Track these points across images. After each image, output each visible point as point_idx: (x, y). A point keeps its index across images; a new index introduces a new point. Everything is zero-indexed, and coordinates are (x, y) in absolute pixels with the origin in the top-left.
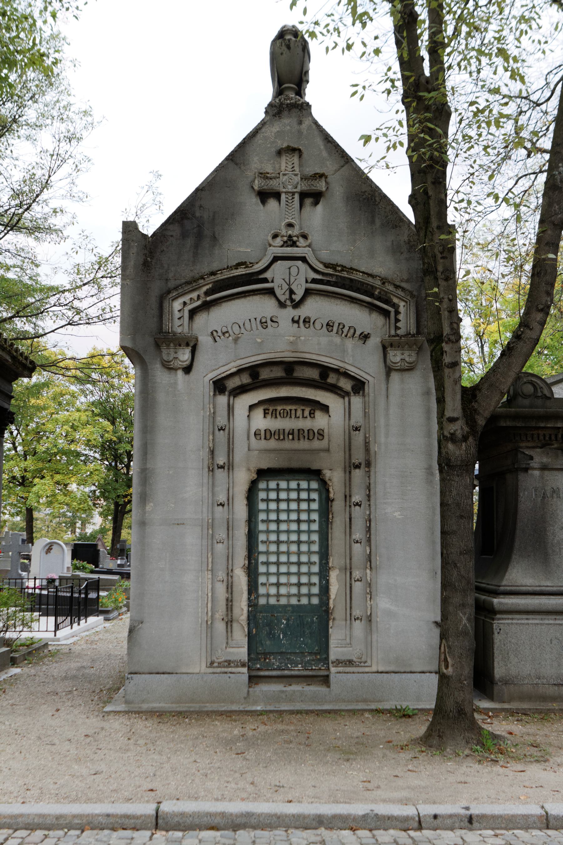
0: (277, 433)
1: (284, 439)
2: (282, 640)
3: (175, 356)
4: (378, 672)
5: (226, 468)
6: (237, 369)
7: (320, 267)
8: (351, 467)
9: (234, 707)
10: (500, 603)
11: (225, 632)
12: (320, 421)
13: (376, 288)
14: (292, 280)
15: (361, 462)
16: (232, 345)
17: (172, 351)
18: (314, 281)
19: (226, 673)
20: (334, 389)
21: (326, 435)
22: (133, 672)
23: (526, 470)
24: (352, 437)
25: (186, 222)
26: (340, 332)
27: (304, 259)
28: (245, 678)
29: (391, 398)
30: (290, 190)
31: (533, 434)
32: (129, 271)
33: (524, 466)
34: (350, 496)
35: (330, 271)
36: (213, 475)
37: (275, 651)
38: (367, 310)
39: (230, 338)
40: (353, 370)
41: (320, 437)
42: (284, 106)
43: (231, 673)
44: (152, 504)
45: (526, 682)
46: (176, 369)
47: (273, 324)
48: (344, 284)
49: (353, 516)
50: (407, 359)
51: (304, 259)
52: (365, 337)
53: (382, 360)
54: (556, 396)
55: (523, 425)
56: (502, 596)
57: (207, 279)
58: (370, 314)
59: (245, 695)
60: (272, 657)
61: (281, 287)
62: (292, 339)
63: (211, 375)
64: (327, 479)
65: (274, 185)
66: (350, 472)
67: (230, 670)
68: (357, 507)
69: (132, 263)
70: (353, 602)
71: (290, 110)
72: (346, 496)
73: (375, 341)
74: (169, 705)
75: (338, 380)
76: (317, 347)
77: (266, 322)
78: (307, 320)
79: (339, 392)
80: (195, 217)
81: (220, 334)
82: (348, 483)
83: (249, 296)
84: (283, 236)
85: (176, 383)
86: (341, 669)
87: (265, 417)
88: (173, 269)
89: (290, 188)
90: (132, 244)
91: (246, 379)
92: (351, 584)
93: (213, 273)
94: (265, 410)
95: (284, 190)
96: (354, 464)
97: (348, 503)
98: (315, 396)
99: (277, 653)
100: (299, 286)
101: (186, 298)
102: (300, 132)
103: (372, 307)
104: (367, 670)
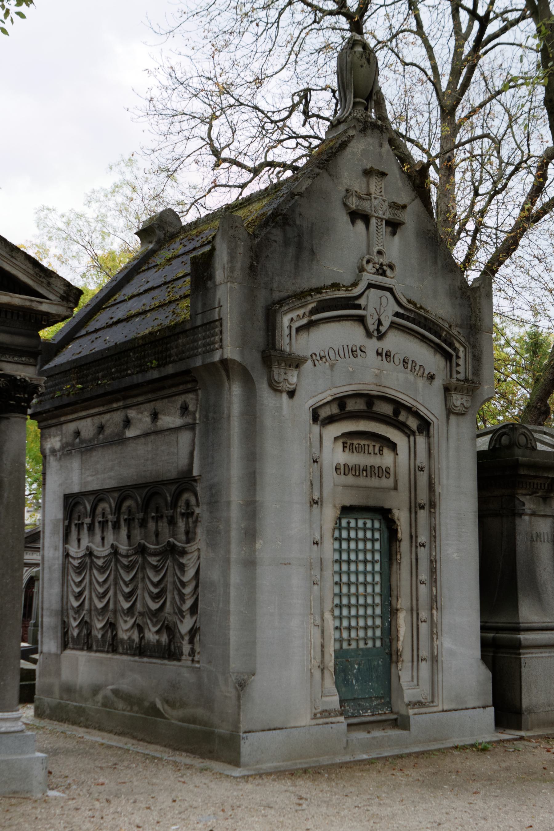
0: (354, 469)
1: (359, 475)
2: (354, 686)
3: (285, 377)
4: (443, 711)
5: (319, 503)
6: (333, 397)
7: (404, 302)
8: (415, 507)
9: (338, 760)
10: (525, 639)
11: (320, 680)
12: (387, 459)
13: (444, 330)
14: (382, 310)
15: (428, 503)
16: (328, 372)
17: (282, 371)
18: (397, 315)
19: (327, 723)
20: (402, 427)
21: (392, 472)
22: (247, 730)
23: (521, 515)
24: (418, 477)
25: (287, 228)
26: (413, 370)
27: (390, 290)
28: (344, 727)
29: (451, 440)
30: (380, 216)
31: (530, 483)
32: (236, 273)
33: (521, 512)
34: (416, 537)
35: (411, 307)
36: (321, 512)
37: (349, 697)
38: (433, 350)
39: (327, 363)
40: (423, 411)
41: (388, 475)
42: (369, 124)
43: (332, 723)
44: (261, 542)
45: (541, 710)
46: (281, 392)
47: (362, 353)
48: (420, 322)
49: (419, 557)
50: (465, 404)
51: (390, 290)
52: (431, 377)
53: (444, 402)
54: (538, 449)
55: (534, 474)
56: (523, 633)
57: (314, 297)
58: (435, 355)
59: (345, 745)
60: (346, 704)
61: (372, 316)
62: (377, 371)
63: (311, 402)
64: (396, 518)
65: (366, 206)
66: (416, 513)
67: (330, 720)
68: (422, 548)
69: (238, 265)
70: (420, 643)
71: (373, 129)
72: (411, 537)
73: (438, 383)
74: (281, 764)
75: (407, 418)
76: (397, 383)
77: (356, 351)
78: (388, 354)
79: (406, 431)
80: (295, 224)
81: (318, 358)
82: (413, 523)
83: (342, 320)
84: (374, 263)
85: (281, 407)
86: (416, 711)
87: (344, 451)
88: (277, 278)
89: (380, 214)
90: (239, 243)
91: (335, 410)
92: (418, 625)
93: (318, 290)
94: (344, 443)
95: (376, 215)
96: (420, 504)
97: (414, 544)
98: (386, 433)
99: (350, 700)
100: (387, 318)
101: (293, 315)
102: (380, 155)
103: (438, 349)
104: (435, 709)
